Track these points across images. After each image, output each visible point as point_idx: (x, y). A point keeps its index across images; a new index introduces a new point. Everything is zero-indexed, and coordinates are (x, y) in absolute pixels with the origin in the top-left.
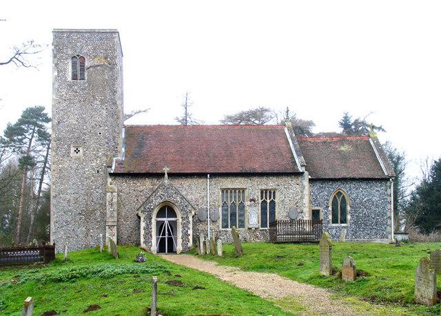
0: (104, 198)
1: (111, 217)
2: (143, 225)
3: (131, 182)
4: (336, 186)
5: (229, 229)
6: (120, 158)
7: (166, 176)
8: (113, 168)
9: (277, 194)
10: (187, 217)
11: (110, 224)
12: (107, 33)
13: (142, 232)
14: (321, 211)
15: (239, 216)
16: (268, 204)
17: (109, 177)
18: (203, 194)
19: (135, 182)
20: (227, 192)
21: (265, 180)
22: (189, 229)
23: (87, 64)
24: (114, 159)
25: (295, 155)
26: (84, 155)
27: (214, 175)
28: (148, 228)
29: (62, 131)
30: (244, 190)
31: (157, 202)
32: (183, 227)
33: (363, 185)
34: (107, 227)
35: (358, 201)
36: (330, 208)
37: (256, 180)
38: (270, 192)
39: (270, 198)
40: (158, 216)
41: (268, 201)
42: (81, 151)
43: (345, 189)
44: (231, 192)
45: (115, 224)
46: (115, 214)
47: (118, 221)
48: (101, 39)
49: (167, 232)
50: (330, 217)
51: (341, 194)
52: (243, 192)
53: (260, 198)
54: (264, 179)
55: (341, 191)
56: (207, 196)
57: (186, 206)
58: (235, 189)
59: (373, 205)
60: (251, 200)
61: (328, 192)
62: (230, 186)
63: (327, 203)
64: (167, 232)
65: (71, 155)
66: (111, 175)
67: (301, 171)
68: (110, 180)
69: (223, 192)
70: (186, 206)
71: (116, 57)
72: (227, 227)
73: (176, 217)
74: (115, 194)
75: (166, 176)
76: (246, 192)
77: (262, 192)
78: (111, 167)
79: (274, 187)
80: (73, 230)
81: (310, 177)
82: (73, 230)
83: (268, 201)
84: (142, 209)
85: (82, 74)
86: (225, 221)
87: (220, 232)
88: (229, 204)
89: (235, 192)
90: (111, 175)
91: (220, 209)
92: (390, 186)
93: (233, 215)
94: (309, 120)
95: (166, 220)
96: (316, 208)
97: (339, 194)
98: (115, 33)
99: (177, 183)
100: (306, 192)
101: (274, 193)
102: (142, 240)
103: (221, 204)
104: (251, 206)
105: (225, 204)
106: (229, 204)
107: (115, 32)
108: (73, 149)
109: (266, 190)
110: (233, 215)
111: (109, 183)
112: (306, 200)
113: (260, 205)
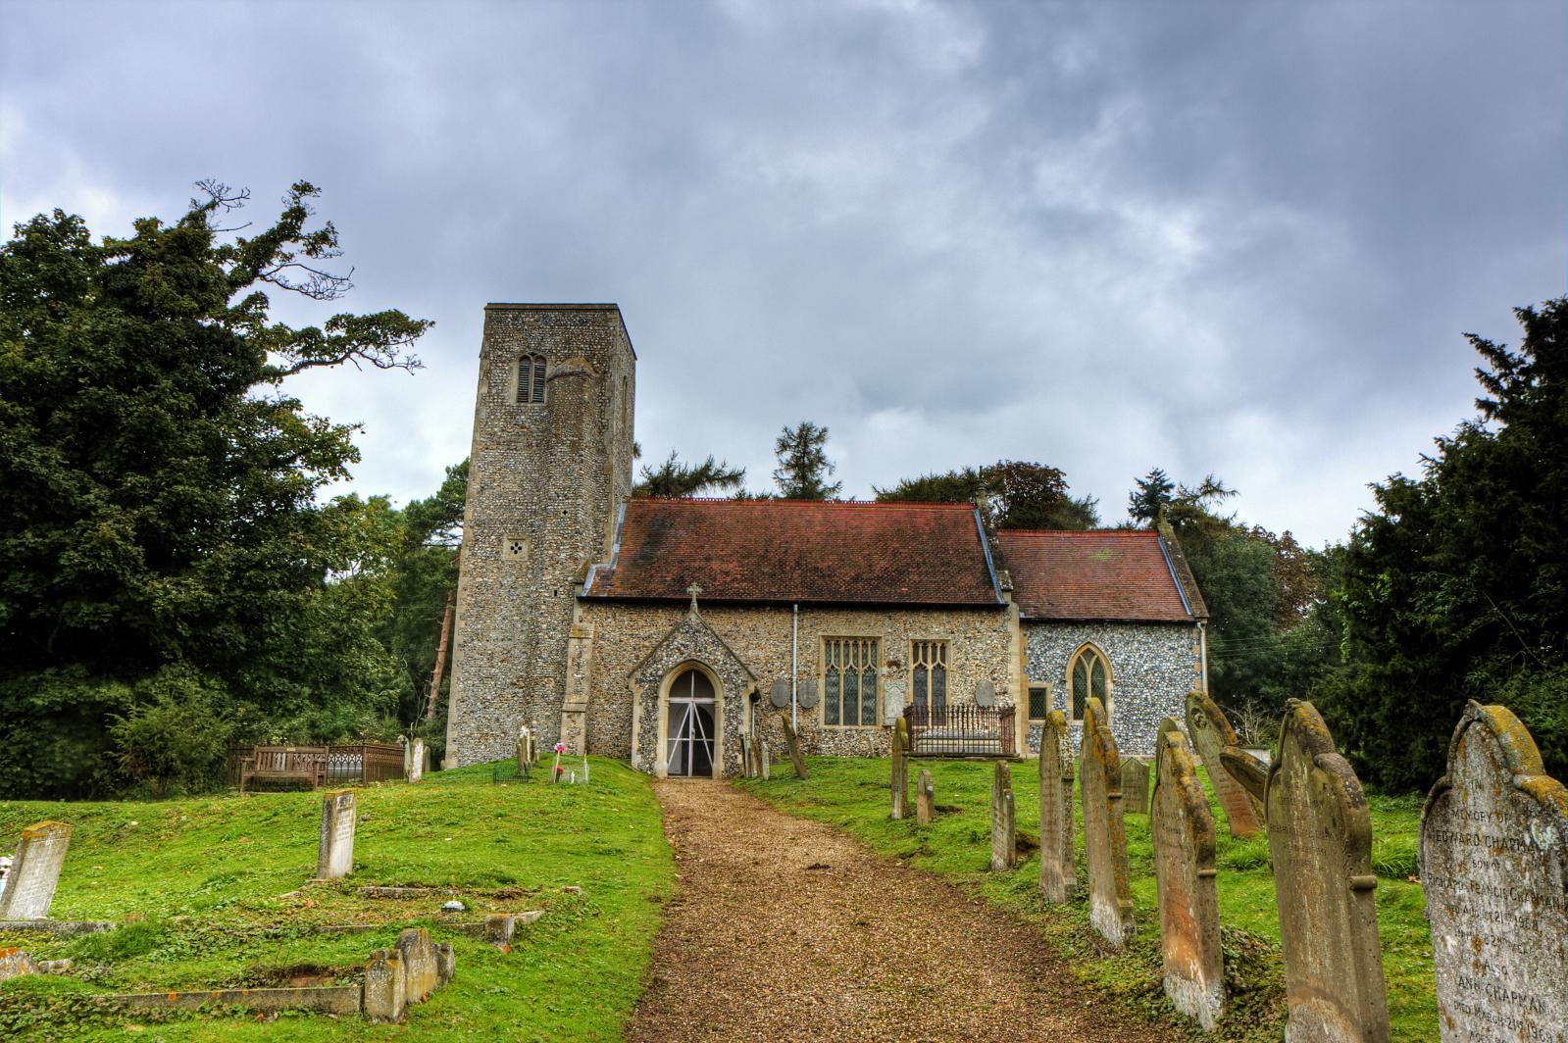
0: (564, 651)
1: (577, 692)
2: (638, 711)
3: (625, 617)
4: (1078, 638)
5: (841, 727)
6: (607, 564)
7: (695, 604)
8: (589, 585)
9: (951, 652)
10: (738, 697)
11: (572, 707)
12: (595, 310)
13: (637, 728)
14: (1048, 690)
15: (864, 698)
16: (930, 673)
17: (576, 606)
18: (783, 648)
19: (634, 617)
20: (837, 644)
21: (923, 620)
22: (741, 723)
23: (550, 371)
24: (594, 567)
25: (991, 568)
26: (530, 557)
27: (807, 607)
28: (649, 715)
29: (488, 508)
30: (875, 641)
31: (671, 660)
32: (728, 719)
33: (1141, 636)
34: (565, 715)
35: (1129, 670)
36: (1069, 685)
37: (903, 620)
38: (934, 647)
39: (934, 661)
40: (673, 692)
41: (930, 667)
42: (525, 549)
43: (1104, 643)
44: (847, 645)
45: (583, 708)
46: (586, 687)
47: (591, 702)
48: (582, 322)
49: (692, 729)
50: (1070, 705)
51: (1093, 654)
52: (874, 644)
53: (911, 659)
54: (921, 618)
55: (1093, 649)
56: (791, 652)
57: (736, 672)
58: (855, 639)
59: (1163, 678)
60: (891, 664)
61: (1063, 649)
62: (844, 632)
63: (1063, 674)
64: (692, 729)
65: (504, 557)
66: (582, 600)
67: (1001, 602)
68: (578, 612)
69: (828, 643)
70: (736, 672)
71: (610, 358)
72: (836, 722)
73: (712, 694)
74: (588, 642)
75: (695, 604)
76: (883, 646)
77: (916, 646)
78: (583, 584)
79: (944, 636)
80: (497, 720)
81: (1022, 615)
82: (497, 720)
83: (930, 667)
84: (638, 674)
85: (539, 392)
86: (832, 708)
87: (819, 733)
88: (842, 670)
89: (856, 645)
90: (582, 600)
91: (822, 681)
92: (1199, 640)
93: (851, 695)
94: (294, 396)
95: (691, 702)
96: (1037, 684)
97: (1089, 653)
98: (610, 310)
99: (722, 623)
100: (1014, 648)
101: (943, 648)
102: (635, 745)
103: (823, 670)
104: (890, 675)
105: (832, 670)
106: (842, 670)
107: (613, 309)
108: (507, 544)
109: (925, 643)
110: (851, 695)
111: (576, 619)
112: (1014, 666)
113: (911, 674)
